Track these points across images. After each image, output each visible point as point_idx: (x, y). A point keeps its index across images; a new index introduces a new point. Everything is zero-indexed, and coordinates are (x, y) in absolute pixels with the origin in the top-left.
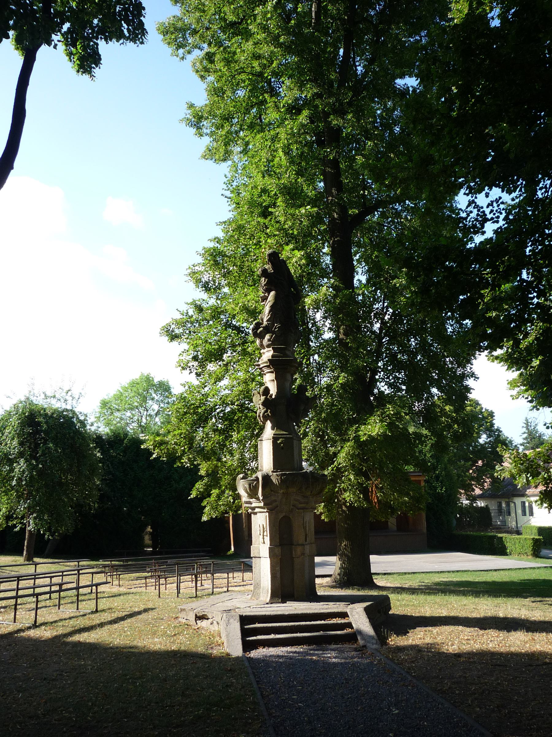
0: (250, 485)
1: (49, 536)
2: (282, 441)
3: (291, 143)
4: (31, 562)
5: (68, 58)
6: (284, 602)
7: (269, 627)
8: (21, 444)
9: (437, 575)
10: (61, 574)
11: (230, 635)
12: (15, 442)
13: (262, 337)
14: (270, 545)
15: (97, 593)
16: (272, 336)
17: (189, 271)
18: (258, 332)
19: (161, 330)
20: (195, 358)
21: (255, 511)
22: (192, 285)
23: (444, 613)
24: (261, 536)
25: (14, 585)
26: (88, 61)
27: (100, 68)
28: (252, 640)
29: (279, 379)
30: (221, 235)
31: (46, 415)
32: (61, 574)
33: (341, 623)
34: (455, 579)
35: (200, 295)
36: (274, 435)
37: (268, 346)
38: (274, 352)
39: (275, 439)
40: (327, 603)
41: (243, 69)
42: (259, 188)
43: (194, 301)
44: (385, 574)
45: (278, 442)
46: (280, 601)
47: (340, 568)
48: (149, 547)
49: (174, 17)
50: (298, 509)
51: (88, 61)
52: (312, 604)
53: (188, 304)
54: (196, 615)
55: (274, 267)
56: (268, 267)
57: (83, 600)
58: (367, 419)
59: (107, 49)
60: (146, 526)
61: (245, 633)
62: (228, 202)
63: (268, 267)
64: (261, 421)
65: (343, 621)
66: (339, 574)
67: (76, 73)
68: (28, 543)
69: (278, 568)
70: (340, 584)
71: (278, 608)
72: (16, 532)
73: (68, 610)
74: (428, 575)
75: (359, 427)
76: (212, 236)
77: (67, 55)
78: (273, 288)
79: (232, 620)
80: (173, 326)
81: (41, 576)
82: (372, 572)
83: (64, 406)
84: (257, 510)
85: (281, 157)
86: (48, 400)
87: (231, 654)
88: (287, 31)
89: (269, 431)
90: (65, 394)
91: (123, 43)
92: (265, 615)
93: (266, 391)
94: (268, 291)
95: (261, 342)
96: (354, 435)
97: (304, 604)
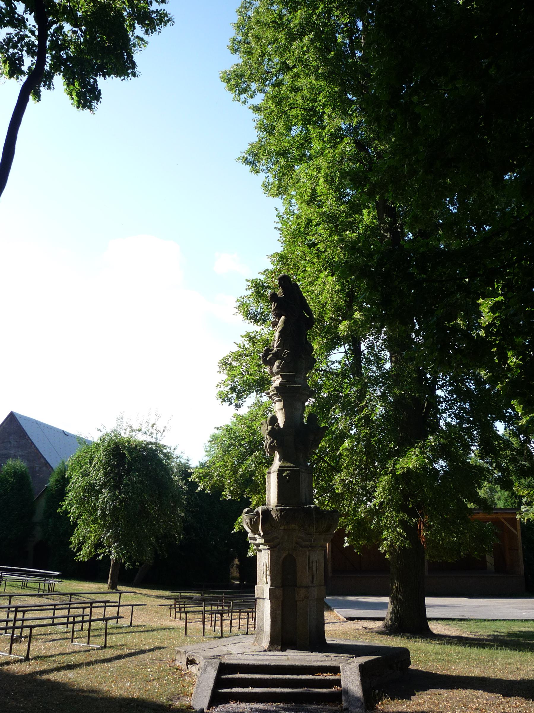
0: (251, 520)
1: (129, 565)
2: (288, 474)
4: (114, 591)
5: (69, 96)
6: (283, 650)
7: (248, 679)
8: (106, 475)
9: (520, 623)
10: (53, 607)
11: (201, 685)
12: (101, 474)
14: (271, 586)
15: (89, 630)
16: (281, 363)
17: (238, 303)
20: (233, 389)
21: (260, 548)
23: (476, 672)
24: (265, 576)
25: (50, 614)
26: (87, 97)
27: (100, 102)
28: (225, 692)
29: (286, 408)
30: (271, 267)
31: (130, 447)
32: (53, 607)
33: (330, 680)
34: (523, 629)
35: (253, 328)
36: (280, 467)
37: (277, 373)
38: (282, 379)
39: (280, 472)
40: (328, 654)
41: (294, 104)
42: (303, 217)
44: (461, 620)
45: (284, 475)
46: (279, 648)
47: (391, 613)
48: (237, 580)
49: (237, 65)
50: (302, 547)
51: (87, 97)
52: (313, 654)
53: (243, 337)
54: (187, 659)
55: (284, 292)
56: (280, 292)
57: (112, 634)
58: (407, 450)
59: (106, 84)
60: (233, 559)
61: (219, 683)
64: (268, 452)
65: (330, 677)
66: (390, 619)
67: (76, 109)
68: (112, 571)
69: (279, 612)
70: (390, 630)
71: (275, 657)
72: (98, 560)
73: (80, 644)
74: (509, 623)
75: (397, 459)
76: (262, 269)
77: (68, 94)
78: (283, 313)
79: (209, 668)
81: (38, 608)
82: (427, 616)
83: (149, 439)
84: (261, 547)
85: (322, 187)
86: (134, 434)
87: (194, 707)
88: (328, 62)
89: (277, 464)
90: (150, 428)
91: (124, 79)
92: (249, 664)
93: (274, 420)
94: (278, 316)
95: (271, 369)
96: (392, 468)
97: (296, 654)
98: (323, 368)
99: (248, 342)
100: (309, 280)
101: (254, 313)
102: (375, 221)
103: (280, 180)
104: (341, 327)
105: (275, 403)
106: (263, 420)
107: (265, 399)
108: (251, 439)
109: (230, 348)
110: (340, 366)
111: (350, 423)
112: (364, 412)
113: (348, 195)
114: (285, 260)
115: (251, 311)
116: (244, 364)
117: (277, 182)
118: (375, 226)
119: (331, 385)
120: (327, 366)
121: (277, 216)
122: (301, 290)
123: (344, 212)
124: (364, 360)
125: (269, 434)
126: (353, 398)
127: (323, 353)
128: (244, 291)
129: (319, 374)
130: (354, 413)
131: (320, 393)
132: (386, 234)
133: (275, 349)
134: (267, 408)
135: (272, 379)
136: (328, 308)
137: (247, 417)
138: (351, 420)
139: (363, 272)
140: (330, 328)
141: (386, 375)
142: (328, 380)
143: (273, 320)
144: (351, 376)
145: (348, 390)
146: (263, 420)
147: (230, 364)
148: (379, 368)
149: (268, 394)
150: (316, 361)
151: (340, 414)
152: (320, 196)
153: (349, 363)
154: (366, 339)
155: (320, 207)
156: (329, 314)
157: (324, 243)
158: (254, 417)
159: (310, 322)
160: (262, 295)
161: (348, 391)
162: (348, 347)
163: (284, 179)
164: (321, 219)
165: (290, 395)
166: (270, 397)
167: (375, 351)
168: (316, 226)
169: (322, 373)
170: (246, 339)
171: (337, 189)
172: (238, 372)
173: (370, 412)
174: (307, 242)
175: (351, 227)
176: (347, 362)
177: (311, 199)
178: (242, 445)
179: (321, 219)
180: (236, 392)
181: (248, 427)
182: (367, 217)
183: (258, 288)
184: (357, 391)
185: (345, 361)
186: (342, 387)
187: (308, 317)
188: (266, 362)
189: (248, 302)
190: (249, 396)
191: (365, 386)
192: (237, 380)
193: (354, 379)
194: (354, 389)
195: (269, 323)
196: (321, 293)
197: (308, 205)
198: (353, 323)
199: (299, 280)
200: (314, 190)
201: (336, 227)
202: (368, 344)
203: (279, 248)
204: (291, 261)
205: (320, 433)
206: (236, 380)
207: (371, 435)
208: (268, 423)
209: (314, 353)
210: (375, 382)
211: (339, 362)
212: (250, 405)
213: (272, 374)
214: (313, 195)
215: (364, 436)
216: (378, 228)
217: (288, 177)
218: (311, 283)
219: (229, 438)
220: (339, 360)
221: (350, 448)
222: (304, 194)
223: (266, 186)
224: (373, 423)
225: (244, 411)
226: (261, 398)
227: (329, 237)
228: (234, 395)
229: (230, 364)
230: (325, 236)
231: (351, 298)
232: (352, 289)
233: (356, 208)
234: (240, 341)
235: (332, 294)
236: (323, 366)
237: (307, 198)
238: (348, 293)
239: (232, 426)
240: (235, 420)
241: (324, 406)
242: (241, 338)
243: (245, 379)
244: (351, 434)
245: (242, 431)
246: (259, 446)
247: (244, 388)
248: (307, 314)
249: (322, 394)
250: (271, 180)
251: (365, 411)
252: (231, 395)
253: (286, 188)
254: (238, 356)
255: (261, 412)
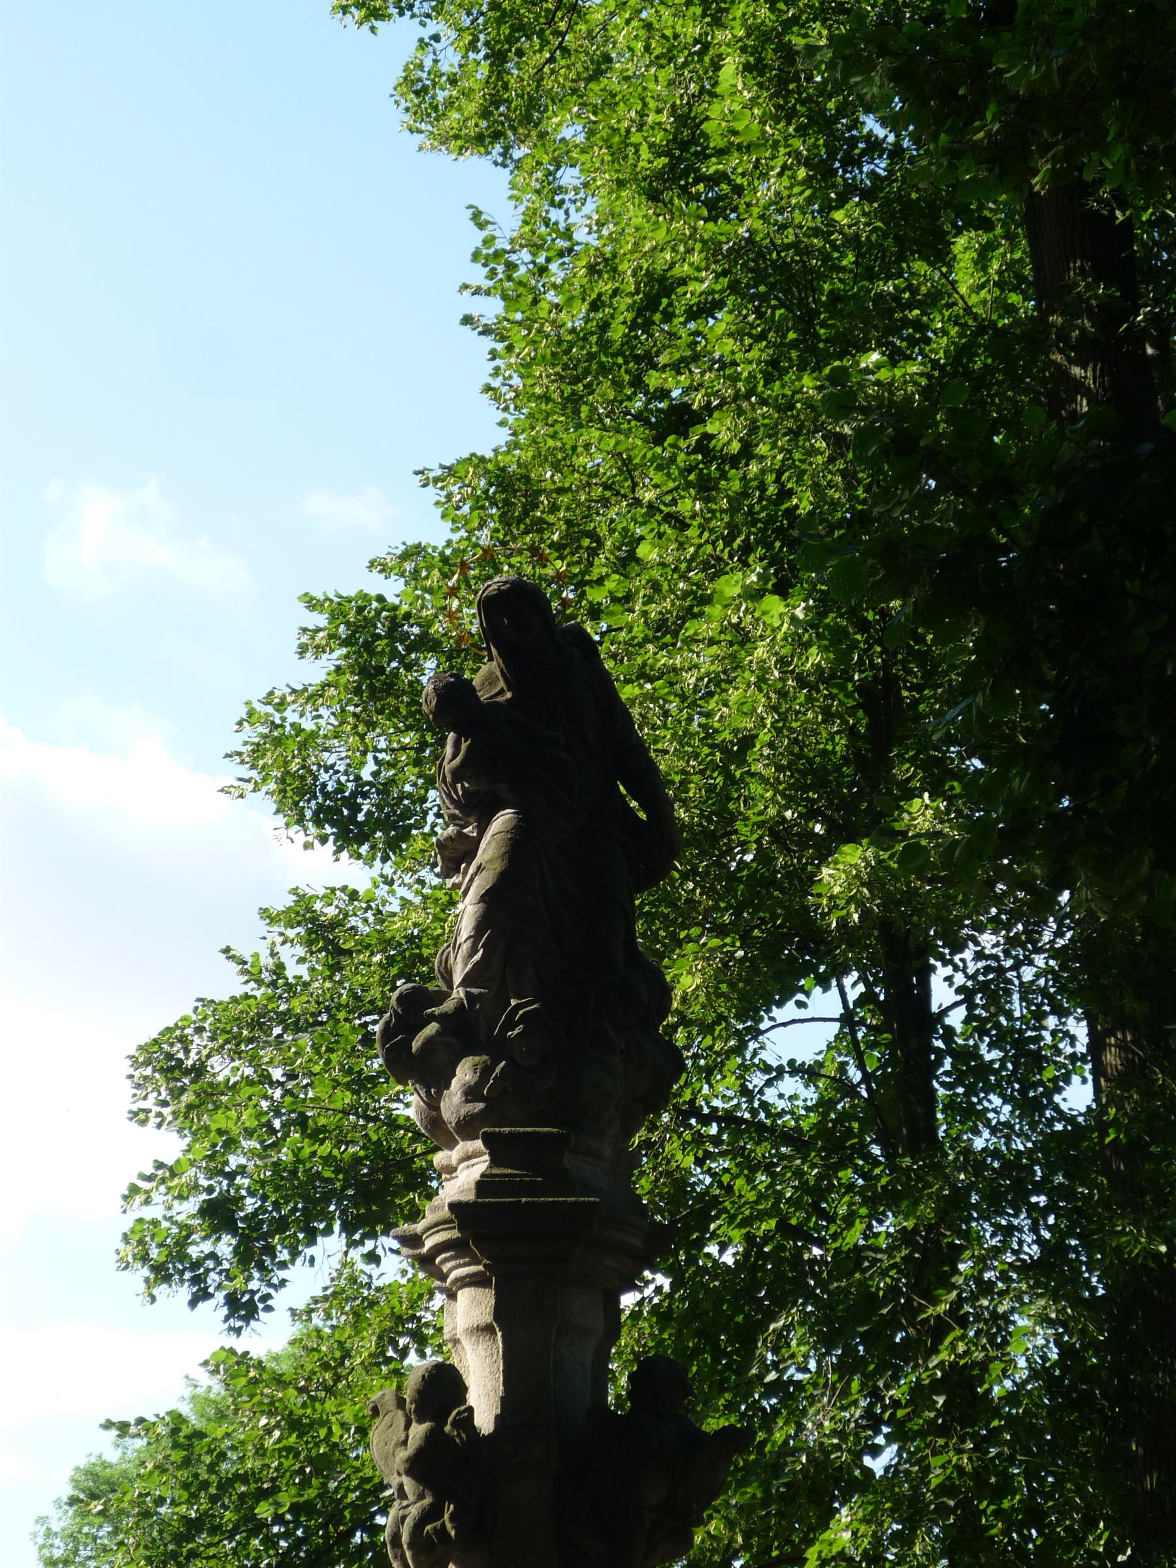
3: (795, 20)
13: (434, 1079)
16: (486, 1071)
17: (252, 734)
18: (416, 1044)
19: (136, 1064)
20: (219, 1214)
22: (261, 811)
29: (511, 1322)
30: (438, 534)
35: (326, 869)
37: (467, 1128)
38: (494, 1162)
42: (625, 267)
43: (303, 900)
55: (514, 672)
56: (486, 676)
62: (494, 355)
63: (486, 676)
76: (389, 544)
80: (200, 1043)
85: (735, 102)
93: (444, 1387)
94: (476, 808)
95: (432, 1104)
98: (717, 1103)
99: (301, 951)
100: (654, 610)
101: (341, 788)
102: (1014, 298)
103: (498, 58)
104: (833, 878)
105: (452, 1296)
106: (381, 1390)
107: (392, 1268)
108: (311, 1493)
109: (198, 977)
110: (810, 1095)
111: (868, 1412)
112: (944, 1355)
113: (874, 146)
114: (519, 502)
115: (324, 776)
116: (277, 1074)
117: (484, 70)
118: (1017, 322)
119: (761, 1197)
120: (745, 1092)
121: (476, 256)
122: (609, 665)
123: (853, 241)
124: (948, 1064)
125: (417, 1467)
126: (884, 1273)
127: (721, 1018)
128: (285, 663)
129: (699, 1139)
130: (891, 1360)
131: (700, 1244)
132: (1077, 371)
133: (459, 993)
134: (399, 1319)
135: (439, 1158)
136: (758, 767)
137: (285, 1368)
138: (876, 1395)
139: (953, 580)
140: (760, 883)
141: (1070, 1147)
142: (750, 1167)
143: (445, 831)
144: (876, 1150)
145: (859, 1226)
146: (381, 1390)
147: (199, 1071)
148: (1031, 1106)
149: (412, 1241)
150: (683, 1067)
151: (812, 1365)
152: (721, 153)
153: (867, 1078)
154: (958, 947)
155: (716, 210)
156: (763, 802)
157: (740, 412)
158: (327, 1369)
159: (656, 845)
160: (391, 686)
161: (854, 1236)
162: (861, 988)
163: (520, 53)
164: (725, 281)
165: (534, 1252)
166: (426, 1262)
167: (1009, 1015)
168: (694, 313)
169: (714, 1129)
170: (291, 933)
171: (820, 122)
172: (248, 1118)
173: (979, 1356)
174: (638, 404)
175: (893, 326)
176: (855, 1075)
177: (672, 167)
178: (258, 1527)
179: (725, 281)
180: (234, 1231)
181: (294, 1424)
182: (973, 272)
183: (368, 647)
184: (905, 1237)
185: (842, 1067)
186: (823, 1214)
187: (642, 815)
188: (403, 1065)
189: (308, 725)
190: (309, 1251)
191: (954, 1208)
192: (243, 1161)
193: (893, 1168)
194: (888, 1225)
195: (420, 844)
196: (718, 683)
197: (654, 196)
198: (904, 858)
199: (595, 613)
200: (687, 123)
201: (806, 322)
202: (972, 977)
203: (485, 432)
204: (554, 508)
205: (700, 1467)
206: (234, 1161)
207: (984, 1482)
208: (410, 1406)
209: (671, 1019)
210: (1006, 1184)
211: (810, 1073)
212: (301, 1305)
213: (438, 1133)
214: (684, 146)
215: (945, 1489)
216: (1034, 335)
217: (545, 43)
218: (665, 631)
219: (186, 1486)
220: (807, 1056)
221: (865, 1555)
222: (636, 138)
223: (418, 90)
224: (997, 1413)
225: (270, 1338)
226: (370, 1268)
227: (769, 380)
228: (225, 1246)
229: (199, 1071)
230: (744, 370)
231: (884, 720)
232: (886, 666)
233: (916, 226)
234: (255, 941)
235: (783, 694)
236: (720, 1095)
237: (648, 162)
238: (861, 688)
239: (195, 1422)
240: (214, 1386)
241: (723, 1317)
242: (262, 927)
243: (285, 1155)
244: (868, 1472)
245: (260, 1451)
246: (351, 1533)
247: (277, 1206)
248: (643, 806)
249: (712, 1249)
250: (450, 60)
251: (953, 1346)
252: (207, 1247)
253: (532, 103)
254: (241, 1027)
255: (369, 1343)
